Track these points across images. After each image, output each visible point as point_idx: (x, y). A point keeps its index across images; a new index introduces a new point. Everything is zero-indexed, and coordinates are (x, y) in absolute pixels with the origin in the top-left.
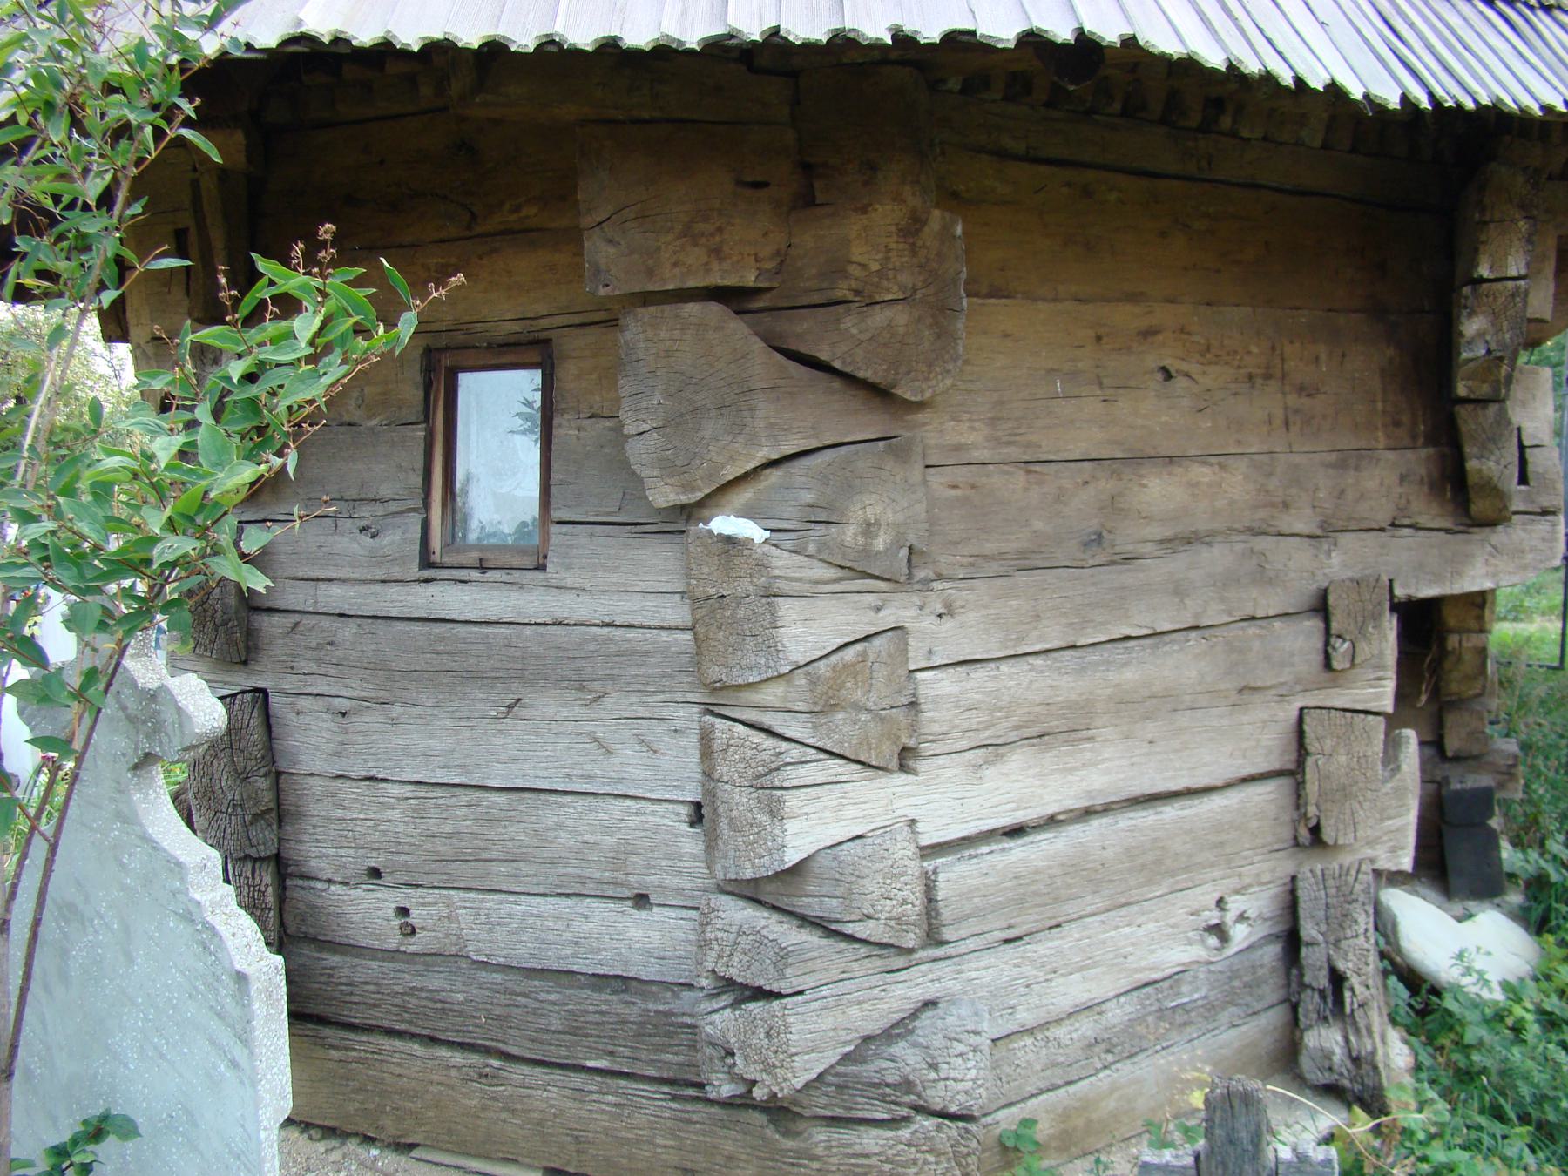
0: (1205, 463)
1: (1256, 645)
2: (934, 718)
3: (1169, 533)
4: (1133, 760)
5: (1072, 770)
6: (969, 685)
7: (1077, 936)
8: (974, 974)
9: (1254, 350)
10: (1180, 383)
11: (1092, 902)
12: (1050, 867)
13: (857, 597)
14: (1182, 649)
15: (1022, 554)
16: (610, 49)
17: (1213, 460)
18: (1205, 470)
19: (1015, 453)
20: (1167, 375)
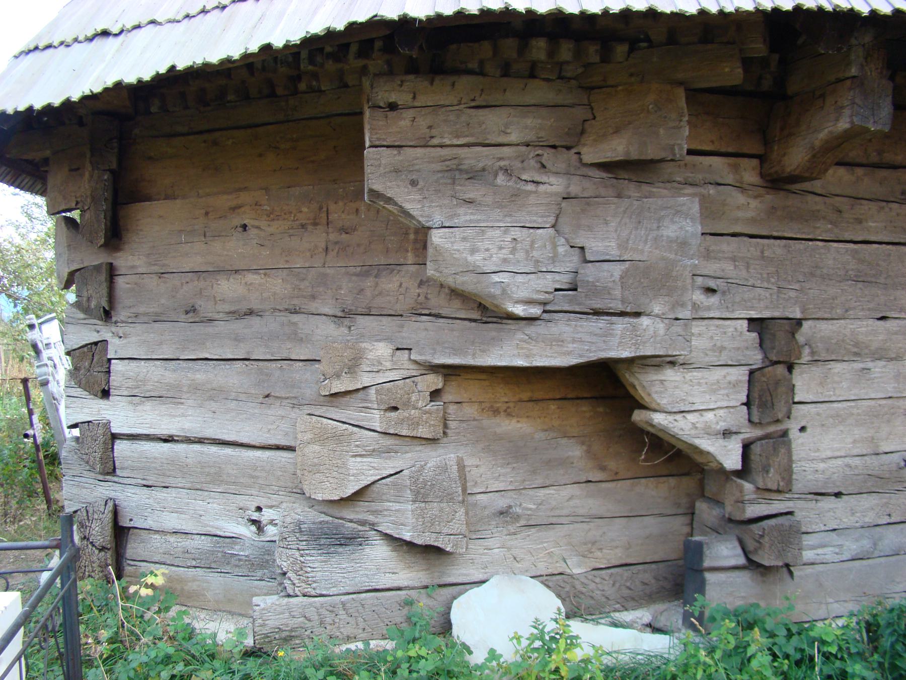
0: (256, 273)
1: (277, 373)
2: (115, 380)
3: (233, 309)
4: (205, 419)
5: (175, 416)
6: (128, 368)
7: (174, 495)
8: (129, 494)
9: (305, 210)
10: (252, 232)
11: (180, 482)
12: (162, 458)
13: (91, 326)
14: (230, 368)
15: (157, 314)
17: (261, 271)
18: (255, 276)
19: (156, 269)
20: (245, 227)
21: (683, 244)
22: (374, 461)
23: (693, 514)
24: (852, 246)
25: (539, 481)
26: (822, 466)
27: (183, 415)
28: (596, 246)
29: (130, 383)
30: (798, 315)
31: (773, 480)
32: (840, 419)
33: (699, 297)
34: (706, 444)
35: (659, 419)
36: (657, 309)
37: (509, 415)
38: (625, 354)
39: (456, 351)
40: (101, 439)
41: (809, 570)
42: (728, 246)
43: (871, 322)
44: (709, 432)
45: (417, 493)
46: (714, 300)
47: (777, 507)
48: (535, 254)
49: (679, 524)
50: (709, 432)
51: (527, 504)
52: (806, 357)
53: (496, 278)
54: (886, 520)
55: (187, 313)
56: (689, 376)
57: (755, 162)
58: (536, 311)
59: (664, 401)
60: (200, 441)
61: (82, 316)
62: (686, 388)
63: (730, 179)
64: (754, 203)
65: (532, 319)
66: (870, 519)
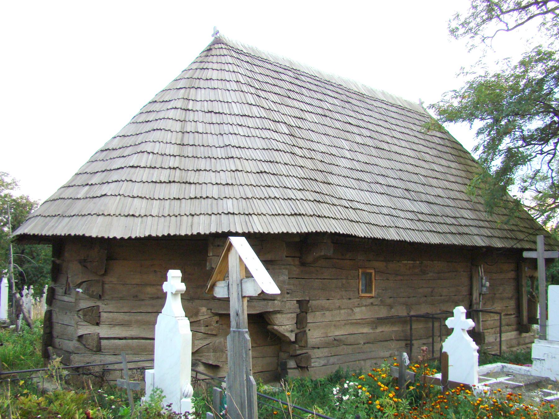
16: (130, 238)
19: (121, 283)
22: (201, 341)
23: (278, 356)
24: (320, 280)
26: (314, 340)
27: (132, 330)
29: (110, 320)
30: (308, 299)
31: (303, 344)
34: (287, 334)
35: (276, 327)
38: (271, 310)
41: (312, 369)
42: (292, 281)
43: (325, 301)
44: (287, 331)
45: (214, 350)
46: (289, 296)
47: (304, 351)
50: (287, 331)
52: (310, 311)
54: (330, 355)
55: (134, 297)
56: (283, 316)
57: (298, 258)
60: (137, 338)
61: (88, 297)
62: (282, 319)
63: (292, 263)
66: (326, 354)
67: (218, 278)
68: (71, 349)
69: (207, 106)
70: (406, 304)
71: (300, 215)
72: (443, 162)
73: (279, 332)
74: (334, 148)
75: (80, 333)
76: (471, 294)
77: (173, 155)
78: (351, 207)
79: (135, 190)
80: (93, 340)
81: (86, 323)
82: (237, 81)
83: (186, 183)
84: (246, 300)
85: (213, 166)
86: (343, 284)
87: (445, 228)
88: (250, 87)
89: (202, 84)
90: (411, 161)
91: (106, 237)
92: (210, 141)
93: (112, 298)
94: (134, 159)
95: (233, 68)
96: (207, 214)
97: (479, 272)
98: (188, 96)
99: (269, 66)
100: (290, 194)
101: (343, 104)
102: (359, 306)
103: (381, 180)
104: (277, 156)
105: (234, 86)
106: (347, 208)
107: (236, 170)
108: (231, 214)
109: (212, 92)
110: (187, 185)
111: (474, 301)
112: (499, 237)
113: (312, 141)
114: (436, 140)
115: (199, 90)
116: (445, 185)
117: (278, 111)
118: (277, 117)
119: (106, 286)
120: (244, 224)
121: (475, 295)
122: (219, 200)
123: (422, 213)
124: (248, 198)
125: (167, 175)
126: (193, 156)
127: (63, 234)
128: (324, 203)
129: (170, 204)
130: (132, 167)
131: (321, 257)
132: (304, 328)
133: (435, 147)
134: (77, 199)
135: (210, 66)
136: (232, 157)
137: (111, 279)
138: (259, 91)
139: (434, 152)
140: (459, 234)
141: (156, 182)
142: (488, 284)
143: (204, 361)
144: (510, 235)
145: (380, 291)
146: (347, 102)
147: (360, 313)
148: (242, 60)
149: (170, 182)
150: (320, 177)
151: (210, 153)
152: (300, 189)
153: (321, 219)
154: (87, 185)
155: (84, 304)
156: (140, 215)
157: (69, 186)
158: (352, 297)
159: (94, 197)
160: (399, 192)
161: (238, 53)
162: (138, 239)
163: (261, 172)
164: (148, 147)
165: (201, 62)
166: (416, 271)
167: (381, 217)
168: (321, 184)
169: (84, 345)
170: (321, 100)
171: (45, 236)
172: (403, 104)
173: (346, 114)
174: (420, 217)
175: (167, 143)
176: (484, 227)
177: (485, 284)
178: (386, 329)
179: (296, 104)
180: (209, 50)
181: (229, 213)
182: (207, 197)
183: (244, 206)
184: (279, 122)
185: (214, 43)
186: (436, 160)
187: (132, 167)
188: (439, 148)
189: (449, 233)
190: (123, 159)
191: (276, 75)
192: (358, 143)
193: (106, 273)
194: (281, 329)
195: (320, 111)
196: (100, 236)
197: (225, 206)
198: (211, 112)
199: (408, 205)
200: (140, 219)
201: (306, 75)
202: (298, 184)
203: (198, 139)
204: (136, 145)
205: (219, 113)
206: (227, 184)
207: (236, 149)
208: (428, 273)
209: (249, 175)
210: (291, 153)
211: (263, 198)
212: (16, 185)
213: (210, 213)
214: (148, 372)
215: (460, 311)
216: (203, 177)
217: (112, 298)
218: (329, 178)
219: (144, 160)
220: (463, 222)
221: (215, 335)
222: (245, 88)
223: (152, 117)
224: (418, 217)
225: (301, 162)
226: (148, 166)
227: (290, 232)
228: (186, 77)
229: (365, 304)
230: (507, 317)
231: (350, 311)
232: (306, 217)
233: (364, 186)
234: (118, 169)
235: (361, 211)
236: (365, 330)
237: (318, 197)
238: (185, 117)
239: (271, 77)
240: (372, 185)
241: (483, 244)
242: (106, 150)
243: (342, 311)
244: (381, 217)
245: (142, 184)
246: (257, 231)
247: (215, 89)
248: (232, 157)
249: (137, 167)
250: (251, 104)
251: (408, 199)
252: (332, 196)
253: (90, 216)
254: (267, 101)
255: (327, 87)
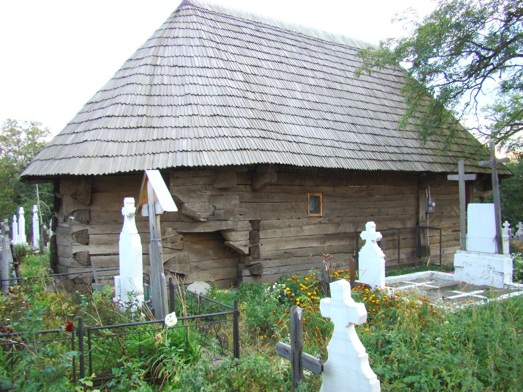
16: (104, 174)
21: (235, 205)
22: (169, 255)
25: (203, 259)
28: (218, 206)
31: (256, 256)
32: (270, 242)
33: (239, 216)
34: (241, 248)
35: (231, 243)
36: (231, 219)
37: (197, 244)
38: (225, 229)
39: (187, 229)
40: (87, 256)
42: (244, 205)
44: (241, 245)
46: (242, 216)
48: (206, 208)
49: (235, 270)
51: (201, 265)
52: (262, 229)
53: (198, 213)
58: (205, 220)
59: (232, 239)
64: (250, 195)
65: (205, 222)
66: (278, 265)
67: (143, 202)
68: (69, 264)
69: (173, 61)
70: (352, 222)
71: (245, 149)
72: (395, 98)
73: (235, 247)
74: (286, 91)
75: (75, 251)
76: (418, 213)
77: (142, 105)
78: (294, 141)
79: (109, 135)
80: (84, 256)
81: (78, 244)
82: (200, 38)
83: (151, 127)
84: (159, 218)
85: (173, 112)
86: (292, 207)
87: (386, 157)
88: (211, 42)
89: (170, 42)
90: (363, 98)
91: (86, 174)
92: (173, 91)
93: (98, 222)
94: (110, 110)
95: (197, 26)
96: (166, 152)
97: (426, 194)
98: (157, 54)
99: (232, 22)
100: (238, 132)
101: (300, 51)
102: (308, 224)
103: (328, 116)
104: (230, 101)
105: (197, 42)
106: (291, 142)
107: (193, 115)
108: (185, 151)
109: (177, 49)
110: (152, 129)
111: (420, 219)
112: (441, 163)
113: (265, 86)
114: (391, 78)
115: (167, 47)
116: (393, 118)
117: (236, 62)
118: (234, 66)
119: (92, 214)
120: (195, 159)
121: (422, 214)
122: (177, 140)
123: (365, 144)
124: (200, 138)
125: (136, 122)
126: (158, 105)
127: (54, 174)
128: (269, 138)
129: (137, 146)
130: (109, 116)
131: (266, 185)
132: (256, 243)
133: (388, 85)
134: (66, 145)
135: (177, 25)
136: (191, 104)
137: (96, 208)
138: (220, 45)
139: (388, 89)
140: (400, 161)
141: (126, 128)
142: (434, 204)
143: (171, 270)
144: (452, 161)
145: (328, 211)
146: (305, 49)
147: (308, 230)
148: (207, 18)
149: (138, 127)
150: (269, 116)
151: (172, 101)
152: (248, 128)
153: (264, 152)
154: (74, 133)
155: (76, 229)
156: (112, 156)
157: (61, 135)
158: (300, 217)
159: (78, 143)
160: (344, 127)
161: (203, 12)
162: (110, 175)
163: (215, 115)
164: (122, 99)
165: (170, 23)
166: (363, 194)
167: (323, 149)
168: (269, 123)
169: (78, 261)
170: (279, 49)
171: (41, 176)
172: (362, 47)
173: (302, 59)
174: (362, 147)
175: (137, 95)
176: (427, 155)
177: (431, 204)
178: (335, 244)
179: (254, 54)
180: (178, 11)
181: (183, 151)
182: (167, 138)
183: (196, 144)
184: (235, 71)
185: (181, 5)
186: (388, 96)
187: (109, 116)
188: (393, 85)
189: (390, 160)
190: (102, 110)
191: (237, 29)
192: (311, 85)
193: (91, 203)
194: (236, 244)
195: (277, 59)
196: (81, 174)
197: (181, 145)
198: (175, 66)
199: (352, 137)
200: (112, 158)
201: (267, 26)
202: (246, 123)
203: (163, 90)
204: (113, 98)
205: (182, 66)
206: (184, 127)
207: (194, 97)
208: (374, 196)
209: (204, 118)
210: (244, 97)
211: (214, 136)
212: (49, 132)
213: (168, 151)
214: (116, 278)
215: (371, 226)
216: (165, 122)
217: (98, 222)
218: (277, 117)
219: (119, 110)
220: (405, 150)
221: (181, 250)
222: (206, 43)
223: (127, 73)
224: (360, 147)
225: (252, 104)
226: (121, 115)
227: (235, 164)
228: (157, 37)
229: (313, 222)
230: (455, 233)
231: (299, 229)
232: (250, 151)
233: (311, 122)
234: (98, 119)
235: (304, 145)
236: (314, 245)
237: (263, 134)
238: (154, 71)
239: (233, 31)
240: (319, 121)
241: (423, 170)
242: (91, 103)
243: (292, 229)
244: (323, 149)
245: (115, 130)
246: (205, 165)
247: (180, 45)
248: (191, 104)
249: (112, 116)
250: (211, 57)
251: (353, 132)
252: (278, 133)
253: (74, 158)
254: (226, 53)
255: (287, 36)
